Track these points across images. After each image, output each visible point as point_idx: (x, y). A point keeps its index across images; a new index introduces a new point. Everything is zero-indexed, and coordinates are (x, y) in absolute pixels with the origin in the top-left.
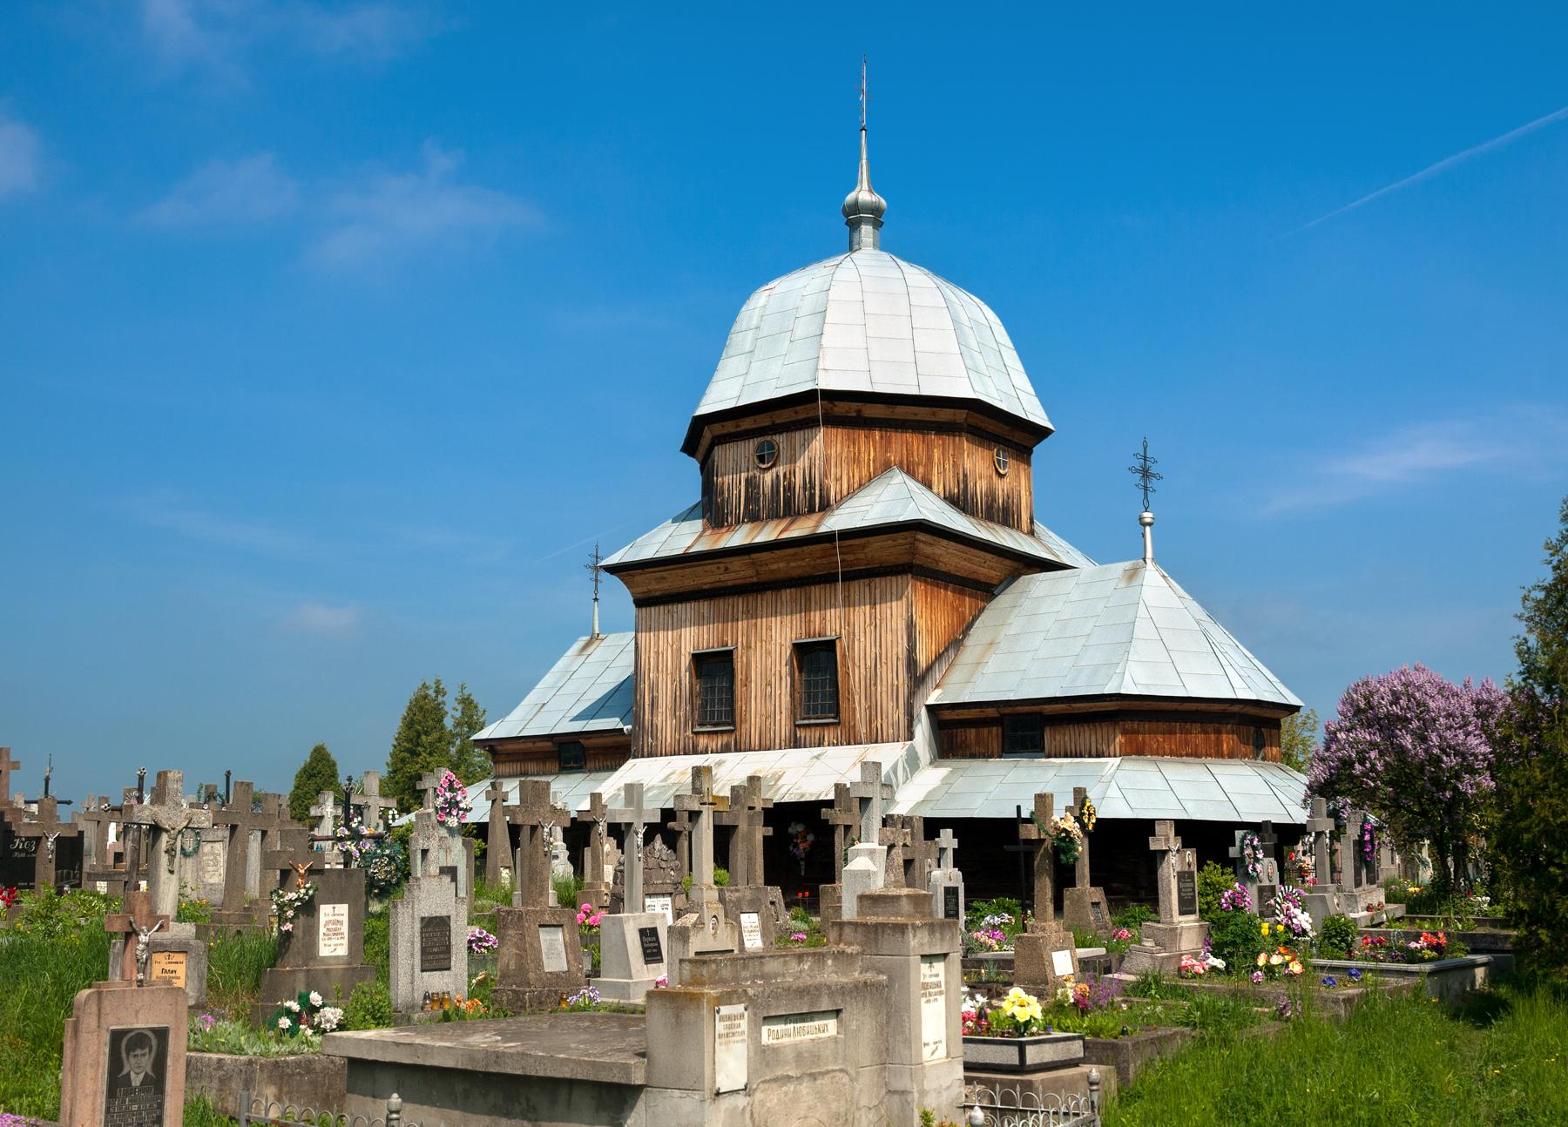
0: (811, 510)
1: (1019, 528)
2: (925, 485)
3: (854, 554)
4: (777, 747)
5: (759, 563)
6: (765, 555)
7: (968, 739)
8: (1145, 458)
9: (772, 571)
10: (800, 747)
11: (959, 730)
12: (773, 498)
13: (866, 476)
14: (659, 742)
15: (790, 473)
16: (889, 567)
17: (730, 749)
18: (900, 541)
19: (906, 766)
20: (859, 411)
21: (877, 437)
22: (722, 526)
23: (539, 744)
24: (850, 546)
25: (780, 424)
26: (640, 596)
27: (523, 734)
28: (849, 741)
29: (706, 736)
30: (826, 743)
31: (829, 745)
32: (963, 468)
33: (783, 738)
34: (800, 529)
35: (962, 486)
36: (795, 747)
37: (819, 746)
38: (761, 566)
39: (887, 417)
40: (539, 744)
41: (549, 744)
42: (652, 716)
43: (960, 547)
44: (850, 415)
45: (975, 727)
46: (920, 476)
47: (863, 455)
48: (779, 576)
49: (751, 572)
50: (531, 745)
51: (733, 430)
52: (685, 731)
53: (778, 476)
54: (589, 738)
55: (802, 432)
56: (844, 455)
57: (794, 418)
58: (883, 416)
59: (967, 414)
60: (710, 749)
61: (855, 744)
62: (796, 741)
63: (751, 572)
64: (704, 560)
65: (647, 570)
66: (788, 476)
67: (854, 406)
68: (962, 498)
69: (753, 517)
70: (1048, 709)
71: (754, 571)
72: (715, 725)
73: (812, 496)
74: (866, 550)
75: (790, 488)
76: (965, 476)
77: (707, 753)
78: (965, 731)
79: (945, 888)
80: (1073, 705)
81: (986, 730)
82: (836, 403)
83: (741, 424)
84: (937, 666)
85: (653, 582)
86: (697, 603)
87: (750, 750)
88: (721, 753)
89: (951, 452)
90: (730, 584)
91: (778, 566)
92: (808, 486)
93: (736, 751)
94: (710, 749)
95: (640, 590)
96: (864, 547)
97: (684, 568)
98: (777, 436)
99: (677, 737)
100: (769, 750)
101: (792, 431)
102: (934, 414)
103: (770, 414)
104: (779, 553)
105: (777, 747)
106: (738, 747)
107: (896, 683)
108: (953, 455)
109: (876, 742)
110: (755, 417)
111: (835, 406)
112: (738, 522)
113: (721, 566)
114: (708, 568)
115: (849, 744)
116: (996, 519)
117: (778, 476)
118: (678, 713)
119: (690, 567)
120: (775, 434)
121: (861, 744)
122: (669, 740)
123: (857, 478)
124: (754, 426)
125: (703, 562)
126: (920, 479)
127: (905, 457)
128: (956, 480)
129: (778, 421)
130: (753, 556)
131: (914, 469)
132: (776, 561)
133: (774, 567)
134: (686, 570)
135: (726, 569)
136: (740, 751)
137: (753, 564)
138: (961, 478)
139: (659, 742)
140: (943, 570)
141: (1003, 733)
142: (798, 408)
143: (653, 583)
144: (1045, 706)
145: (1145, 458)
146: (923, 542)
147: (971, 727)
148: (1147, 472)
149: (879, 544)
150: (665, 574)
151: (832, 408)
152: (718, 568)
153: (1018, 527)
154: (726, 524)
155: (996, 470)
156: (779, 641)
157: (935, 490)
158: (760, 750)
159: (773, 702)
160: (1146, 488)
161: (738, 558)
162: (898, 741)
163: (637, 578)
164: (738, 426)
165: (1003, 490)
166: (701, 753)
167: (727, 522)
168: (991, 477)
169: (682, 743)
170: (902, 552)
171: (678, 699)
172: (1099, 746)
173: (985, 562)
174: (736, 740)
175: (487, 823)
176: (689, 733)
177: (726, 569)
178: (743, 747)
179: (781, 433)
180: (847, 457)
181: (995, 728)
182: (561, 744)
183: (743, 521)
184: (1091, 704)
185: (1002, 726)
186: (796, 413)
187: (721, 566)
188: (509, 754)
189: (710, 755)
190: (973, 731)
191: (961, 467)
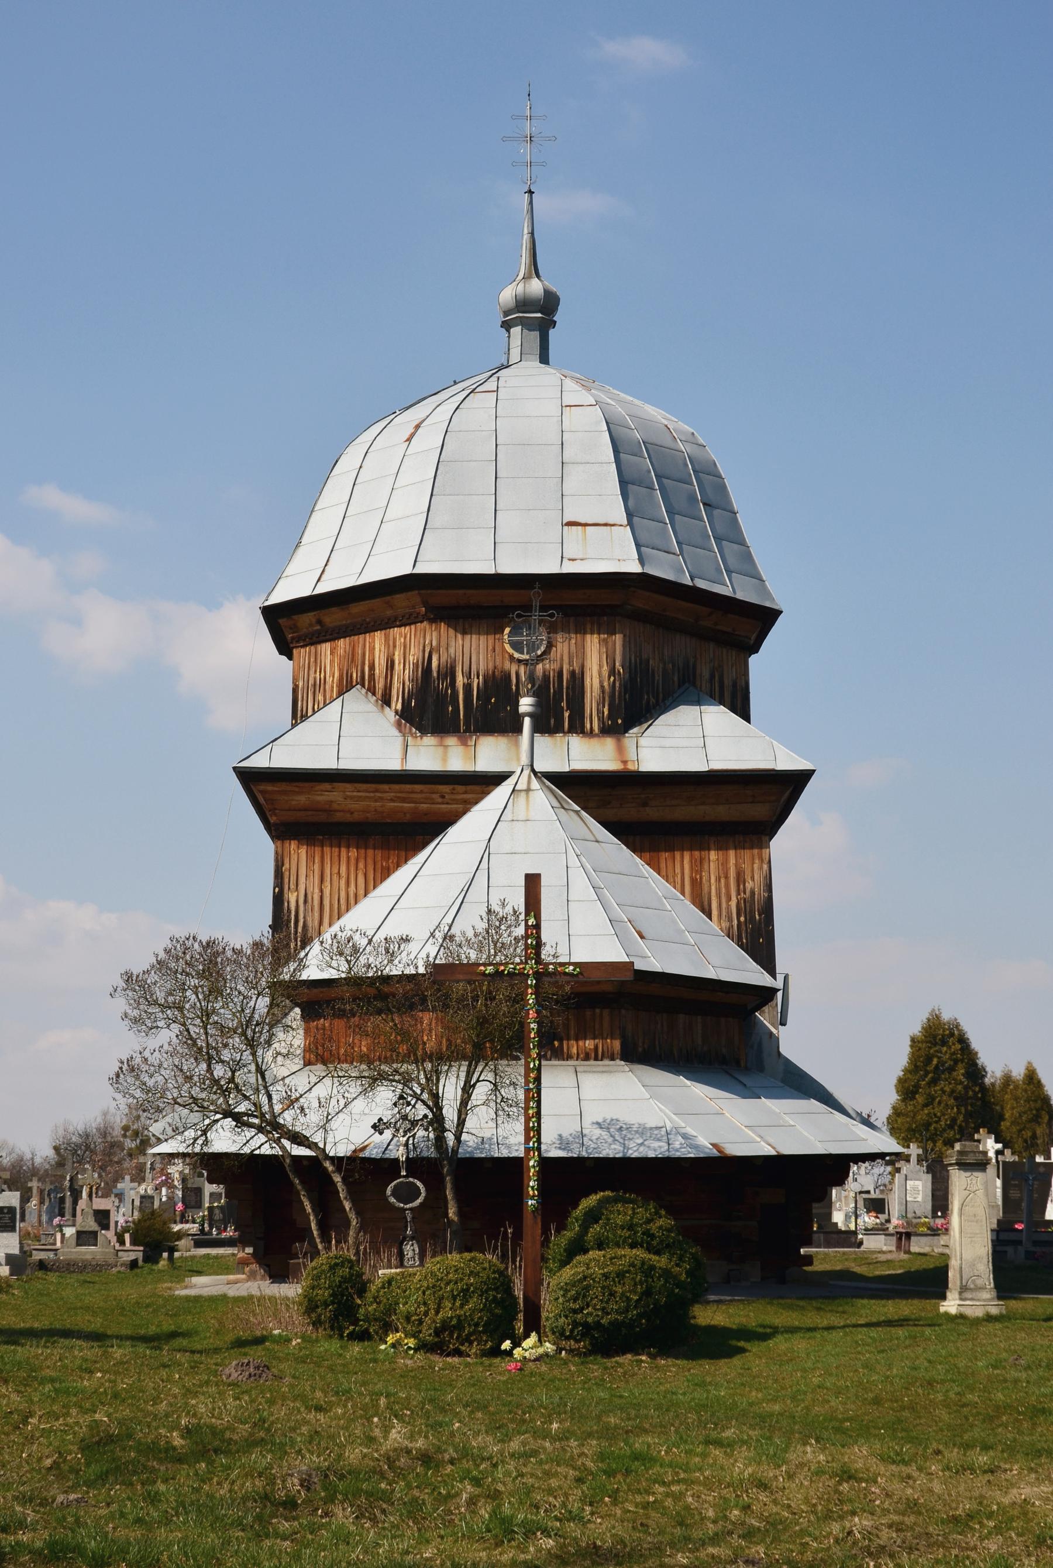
82: (295, 617)
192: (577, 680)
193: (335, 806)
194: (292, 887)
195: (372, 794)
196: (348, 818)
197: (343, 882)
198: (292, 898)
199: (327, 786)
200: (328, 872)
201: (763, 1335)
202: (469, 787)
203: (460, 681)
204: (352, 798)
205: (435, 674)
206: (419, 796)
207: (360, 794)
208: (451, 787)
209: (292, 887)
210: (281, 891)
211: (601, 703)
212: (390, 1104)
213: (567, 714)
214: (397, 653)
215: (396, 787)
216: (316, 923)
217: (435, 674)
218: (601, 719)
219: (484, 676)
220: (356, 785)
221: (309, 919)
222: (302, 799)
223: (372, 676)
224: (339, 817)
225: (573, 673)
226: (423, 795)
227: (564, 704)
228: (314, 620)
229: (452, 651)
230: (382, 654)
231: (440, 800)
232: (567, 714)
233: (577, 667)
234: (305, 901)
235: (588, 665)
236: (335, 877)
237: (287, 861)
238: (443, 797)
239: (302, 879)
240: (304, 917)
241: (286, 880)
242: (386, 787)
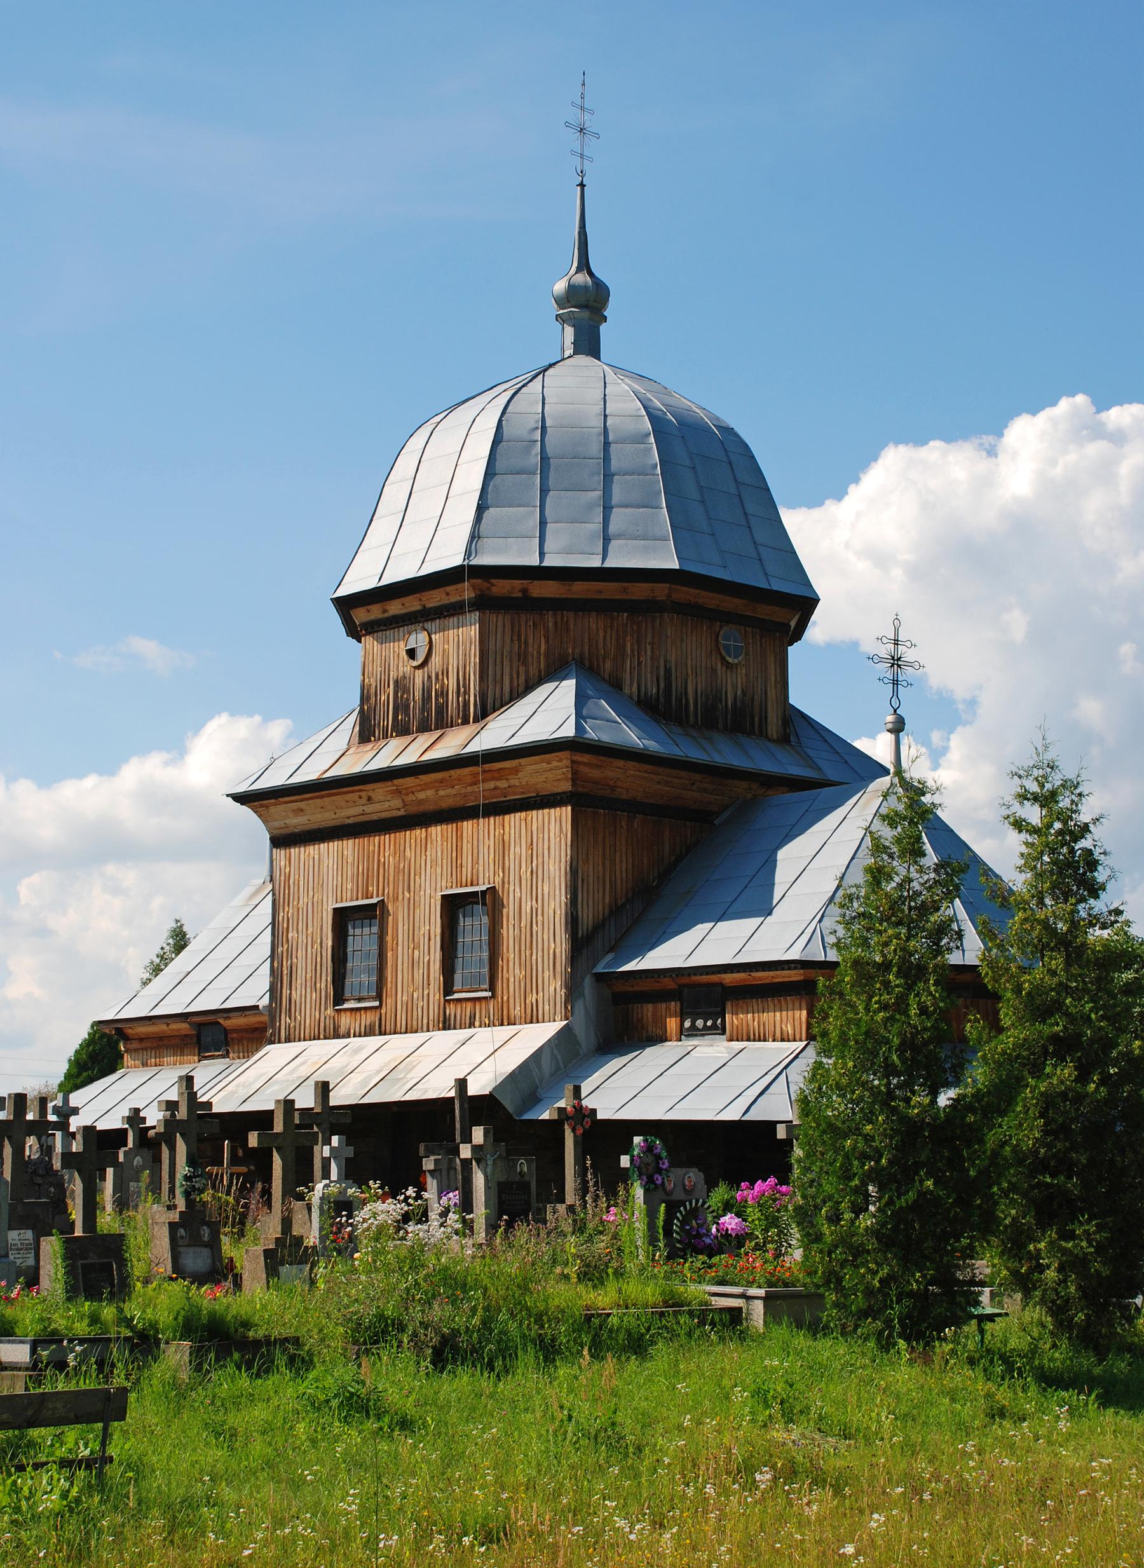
0: (466, 722)
1: (762, 733)
2: (612, 685)
3: (507, 780)
4: (425, 1028)
5: (404, 792)
6: (409, 782)
7: (645, 1017)
8: (896, 642)
9: (420, 802)
10: (449, 1029)
11: (635, 1005)
12: (423, 704)
13: (534, 675)
14: (298, 1023)
15: (443, 674)
16: (558, 794)
17: (374, 1031)
18: (555, 764)
19: (556, 1052)
20: (524, 591)
21: (550, 624)
22: (369, 741)
23: (174, 1026)
24: (501, 769)
25: (431, 608)
26: (276, 832)
27: (159, 1011)
28: (502, 1020)
29: (348, 1014)
30: (477, 1024)
31: (480, 1026)
32: (666, 662)
33: (431, 1018)
34: (451, 744)
35: (662, 685)
36: (444, 1029)
37: (470, 1027)
38: (407, 794)
39: (563, 596)
40: (174, 1026)
41: (185, 1026)
42: (291, 989)
43: (647, 767)
44: (514, 595)
45: (652, 1003)
46: (607, 672)
47: (531, 649)
48: (430, 807)
49: (397, 803)
50: (164, 1027)
51: (380, 616)
52: (326, 1009)
53: (429, 677)
54: (228, 1018)
55: (455, 619)
56: (507, 648)
57: (446, 600)
58: (557, 596)
59: (670, 589)
60: (352, 1032)
61: (508, 1025)
62: (444, 1022)
63: (397, 803)
64: (343, 787)
65: (281, 799)
66: (440, 677)
67: (518, 584)
68: (662, 700)
69: (402, 730)
70: (729, 978)
71: (400, 801)
72: (359, 1000)
73: (466, 704)
74: (520, 775)
75: (443, 693)
76: (668, 671)
77: (349, 1037)
78: (642, 1007)
79: (123, 1235)
80: (753, 974)
81: (664, 1005)
82: (494, 581)
83: (388, 607)
84: (613, 922)
85: (291, 815)
86: (340, 842)
87: (395, 1033)
88: (365, 1035)
89: (649, 639)
90: (375, 817)
91: (427, 794)
92: (462, 690)
93: (380, 1034)
94: (352, 1032)
95: (277, 824)
96: (516, 771)
97: (322, 797)
98: (430, 623)
99: (317, 1016)
100: (416, 1032)
101: (445, 617)
102: (625, 590)
103: (418, 595)
104: (455, 773)
105: (297, 1039)
106: (383, 1028)
107: (553, 945)
108: (652, 644)
109: (531, 1022)
110: (403, 600)
111: (493, 585)
112: (385, 737)
113: (363, 794)
114: (349, 797)
115: (502, 1024)
116: (721, 726)
117: (429, 677)
118: (318, 985)
119: (318, 797)
120: (427, 621)
121: (515, 1024)
122: (308, 1022)
123: (522, 679)
124: (403, 611)
125: (341, 790)
126: (607, 677)
127: (587, 648)
128: (655, 679)
129: (429, 605)
130: (396, 782)
131: (598, 665)
132: (424, 787)
133: (421, 795)
134: (325, 799)
135: (369, 799)
136: (385, 1034)
137: (398, 792)
138: (662, 673)
139: (298, 1023)
140: (624, 797)
141: (681, 1010)
142: (449, 589)
143: (296, 819)
144: (723, 976)
145: (896, 642)
146: (585, 764)
147: (661, 1002)
148: (899, 659)
149: (533, 767)
150: (302, 805)
151: (489, 588)
152: (360, 797)
153: (761, 733)
154: (373, 739)
155: (723, 658)
156: (428, 892)
157: (627, 690)
158: (406, 1032)
159: (421, 971)
160: (895, 682)
161: (379, 785)
162: (554, 1021)
163: (273, 810)
164: (385, 611)
165: (735, 688)
166: (344, 1037)
167: (374, 737)
168: (714, 670)
169: (322, 1025)
170: (559, 777)
171: (318, 968)
172: (784, 1028)
173: (693, 784)
174: (380, 1020)
175: (272, 1112)
176: (330, 1011)
177: (369, 799)
178: (388, 1030)
179: (433, 620)
180: (511, 652)
181: (673, 1003)
182: (200, 1025)
183: (392, 736)
184: (771, 973)
185: (680, 1000)
186: (448, 594)
187: (363, 794)
188: (141, 1040)
189: (352, 1040)
190: (650, 1006)
191: (662, 660)
195: (647, 775)
242: (660, 770)
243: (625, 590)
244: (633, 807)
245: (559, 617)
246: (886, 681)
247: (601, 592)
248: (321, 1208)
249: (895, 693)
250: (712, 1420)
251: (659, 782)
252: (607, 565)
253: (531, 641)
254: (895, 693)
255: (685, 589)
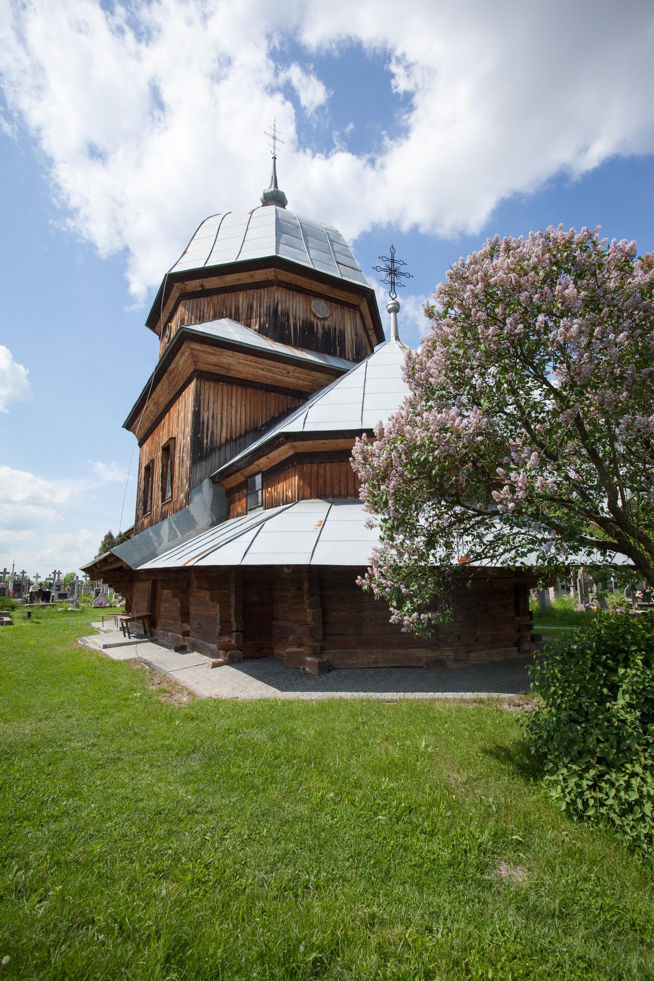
8: (393, 261)
82: (186, 283)
145: (393, 261)
151: (185, 288)
192: (342, 334)
193: (232, 367)
194: (206, 408)
195: (253, 364)
196: (238, 376)
197: (234, 410)
198: (205, 415)
199: (230, 353)
200: (225, 403)
201: (100, 555)
202: (303, 370)
203: (291, 321)
204: (242, 363)
205: (280, 313)
206: (277, 370)
207: (247, 362)
208: (295, 368)
209: (206, 408)
210: (199, 410)
211: (352, 347)
212: (582, 562)
213: (338, 348)
214: (255, 302)
215: (267, 361)
216: (219, 431)
217: (280, 313)
218: (352, 355)
219: (302, 321)
220: (246, 356)
221: (215, 428)
222: (213, 359)
223: (237, 309)
224: (232, 374)
225: (340, 330)
226: (279, 370)
227: (337, 343)
228: (198, 285)
229: (287, 304)
230: (244, 303)
231: (287, 375)
232: (338, 348)
233: (342, 328)
234: (213, 418)
235: (346, 328)
236: (229, 407)
237: (202, 393)
238: (288, 373)
239: (211, 405)
240: (212, 427)
241: (202, 404)
242: (261, 360)
243: (252, 277)
244: (244, 383)
245: (220, 298)
246: (386, 282)
247: (240, 280)
248: (137, 661)
249: (393, 254)
250: (535, 818)
251: (263, 369)
252: (305, 430)
253: (206, 311)
254: (393, 254)
255: (285, 272)
